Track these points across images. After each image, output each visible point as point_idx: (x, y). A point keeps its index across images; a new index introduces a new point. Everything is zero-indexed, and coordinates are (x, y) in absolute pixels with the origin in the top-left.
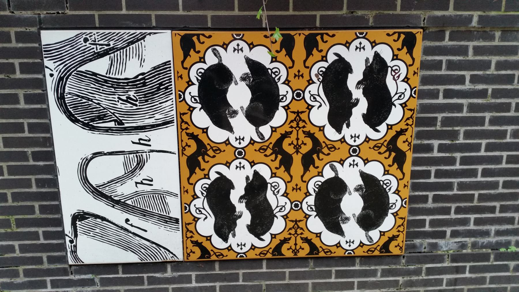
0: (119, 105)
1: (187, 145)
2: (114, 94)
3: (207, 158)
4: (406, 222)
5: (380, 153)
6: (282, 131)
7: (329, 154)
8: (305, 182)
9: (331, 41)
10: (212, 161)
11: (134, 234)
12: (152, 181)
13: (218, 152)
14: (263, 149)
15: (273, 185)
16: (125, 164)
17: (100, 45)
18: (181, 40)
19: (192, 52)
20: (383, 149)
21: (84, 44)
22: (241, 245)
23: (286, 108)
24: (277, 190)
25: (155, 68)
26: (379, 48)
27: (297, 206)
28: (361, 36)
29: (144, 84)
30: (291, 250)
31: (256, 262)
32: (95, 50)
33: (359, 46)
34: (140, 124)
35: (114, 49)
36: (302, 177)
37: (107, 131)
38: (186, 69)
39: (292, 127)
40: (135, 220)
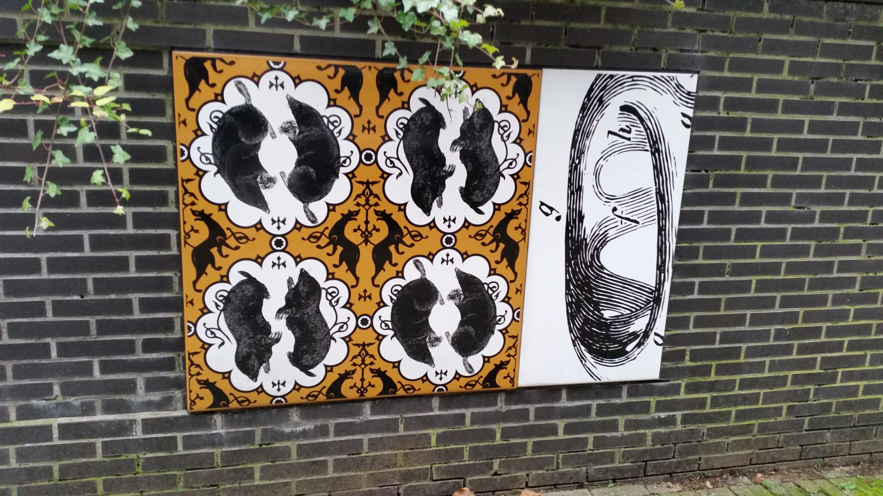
3: (401, 247)
6: (507, 209)
7: (412, 245)
8: (378, 286)
10: (234, 255)
13: (419, 238)
14: (315, 237)
20: (488, 238)
24: (335, 299)
27: (365, 321)
30: (355, 389)
36: (373, 278)
38: (382, 117)
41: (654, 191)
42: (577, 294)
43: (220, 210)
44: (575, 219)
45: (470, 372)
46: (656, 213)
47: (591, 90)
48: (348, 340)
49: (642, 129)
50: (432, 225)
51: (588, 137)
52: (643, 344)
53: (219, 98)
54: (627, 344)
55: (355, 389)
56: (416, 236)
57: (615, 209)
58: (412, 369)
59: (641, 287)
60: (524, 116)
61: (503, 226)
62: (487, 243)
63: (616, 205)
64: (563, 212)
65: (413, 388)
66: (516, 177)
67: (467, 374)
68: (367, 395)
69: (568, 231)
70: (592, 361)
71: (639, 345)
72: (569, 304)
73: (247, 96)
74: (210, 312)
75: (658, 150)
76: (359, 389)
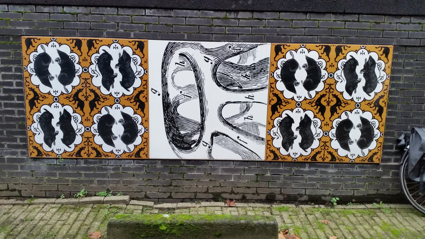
0: (242, 79)
1: (272, 99)
2: (239, 73)
3: (100, 102)
4: (382, 145)
5: (312, 106)
6: (321, 94)
7: (344, 107)
8: (331, 121)
9: (349, 49)
10: (284, 108)
11: (241, 144)
12: (252, 117)
13: (288, 103)
14: (311, 103)
15: (314, 122)
16: (241, 108)
17: (236, 49)
18: (87, 42)
19: (92, 48)
20: (372, 105)
21: (229, 49)
22: (295, 154)
23: (80, 76)
24: (316, 125)
25: (260, 61)
26: (126, 48)
27: (326, 134)
28: (303, 46)
29: (254, 69)
30: (321, 158)
31: (302, 164)
32: (233, 52)
33: (302, 51)
34: (250, 88)
35: (242, 52)
36: (330, 118)
37: (234, 91)
38: (89, 56)
39: (326, 92)
40: (242, 137)
41: (196, 86)
42: (169, 124)
43: (98, 89)
44: (166, 95)
45: (364, 155)
46: (198, 94)
47: (167, 48)
48: (320, 140)
49: (189, 62)
50: (352, 100)
51: (168, 65)
52: (198, 145)
53: (36, 51)
54: (191, 145)
55: (321, 158)
56: (287, 102)
57: (181, 92)
58: (342, 152)
59: (195, 123)
60: (328, 60)
61: (138, 96)
62: (372, 107)
63: (181, 90)
64: (161, 92)
65: (342, 160)
66: (141, 78)
67: (362, 156)
68: (91, 157)
69: (163, 100)
70: (178, 150)
71: (196, 145)
72: (166, 128)
73: (44, 50)
74: (275, 127)
75: (196, 70)
76: (323, 158)
